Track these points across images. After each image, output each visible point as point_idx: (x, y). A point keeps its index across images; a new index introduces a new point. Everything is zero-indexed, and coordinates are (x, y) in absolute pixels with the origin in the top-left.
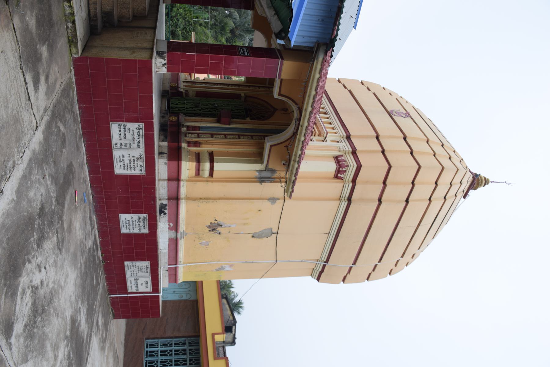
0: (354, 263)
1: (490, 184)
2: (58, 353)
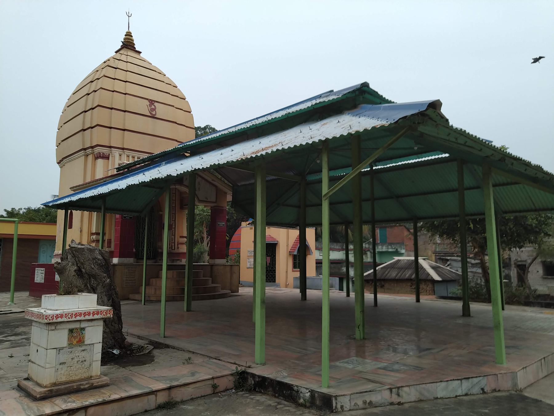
0: (173, 106)
1: (130, 30)
2: (253, 375)
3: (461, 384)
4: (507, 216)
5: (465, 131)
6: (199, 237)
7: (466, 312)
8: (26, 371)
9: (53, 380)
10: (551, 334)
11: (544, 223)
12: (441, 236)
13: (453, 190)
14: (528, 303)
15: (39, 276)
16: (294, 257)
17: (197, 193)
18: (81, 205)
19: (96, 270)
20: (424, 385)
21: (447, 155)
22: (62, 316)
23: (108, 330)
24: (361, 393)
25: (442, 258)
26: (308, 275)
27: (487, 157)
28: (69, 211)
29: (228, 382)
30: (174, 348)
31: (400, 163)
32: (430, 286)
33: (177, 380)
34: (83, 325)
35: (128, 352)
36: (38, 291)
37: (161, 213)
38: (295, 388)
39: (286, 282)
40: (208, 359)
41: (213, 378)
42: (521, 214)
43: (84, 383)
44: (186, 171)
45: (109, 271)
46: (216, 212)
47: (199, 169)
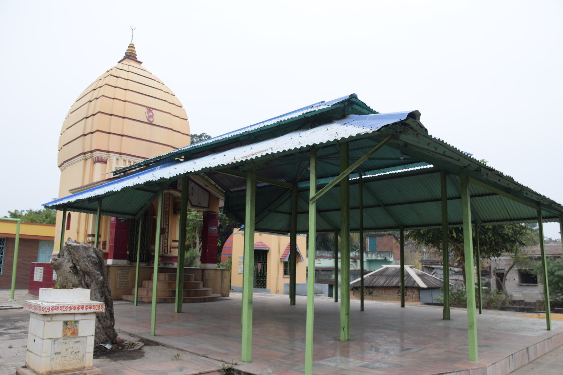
0: (170, 114)
1: (133, 43)
4: (489, 226)
5: (443, 141)
6: (192, 242)
7: (446, 316)
8: (23, 361)
9: (49, 369)
10: (520, 334)
12: (426, 244)
13: (437, 200)
16: (286, 264)
17: (190, 198)
19: (90, 268)
21: (432, 166)
22: (57, 308)
23: (100, 326)
25: (428, 267)
26: (297, 281)
27: (465, 167)
30: (163, 345)
32: (416, 292)
34: (77, 318)
35: (120, 348)
36: (34, 288)
37: (155, 217)
39: (277, 288)
42: (498, 223)
45: (102, 269)
46: (209, 218)
47: (191, 172)
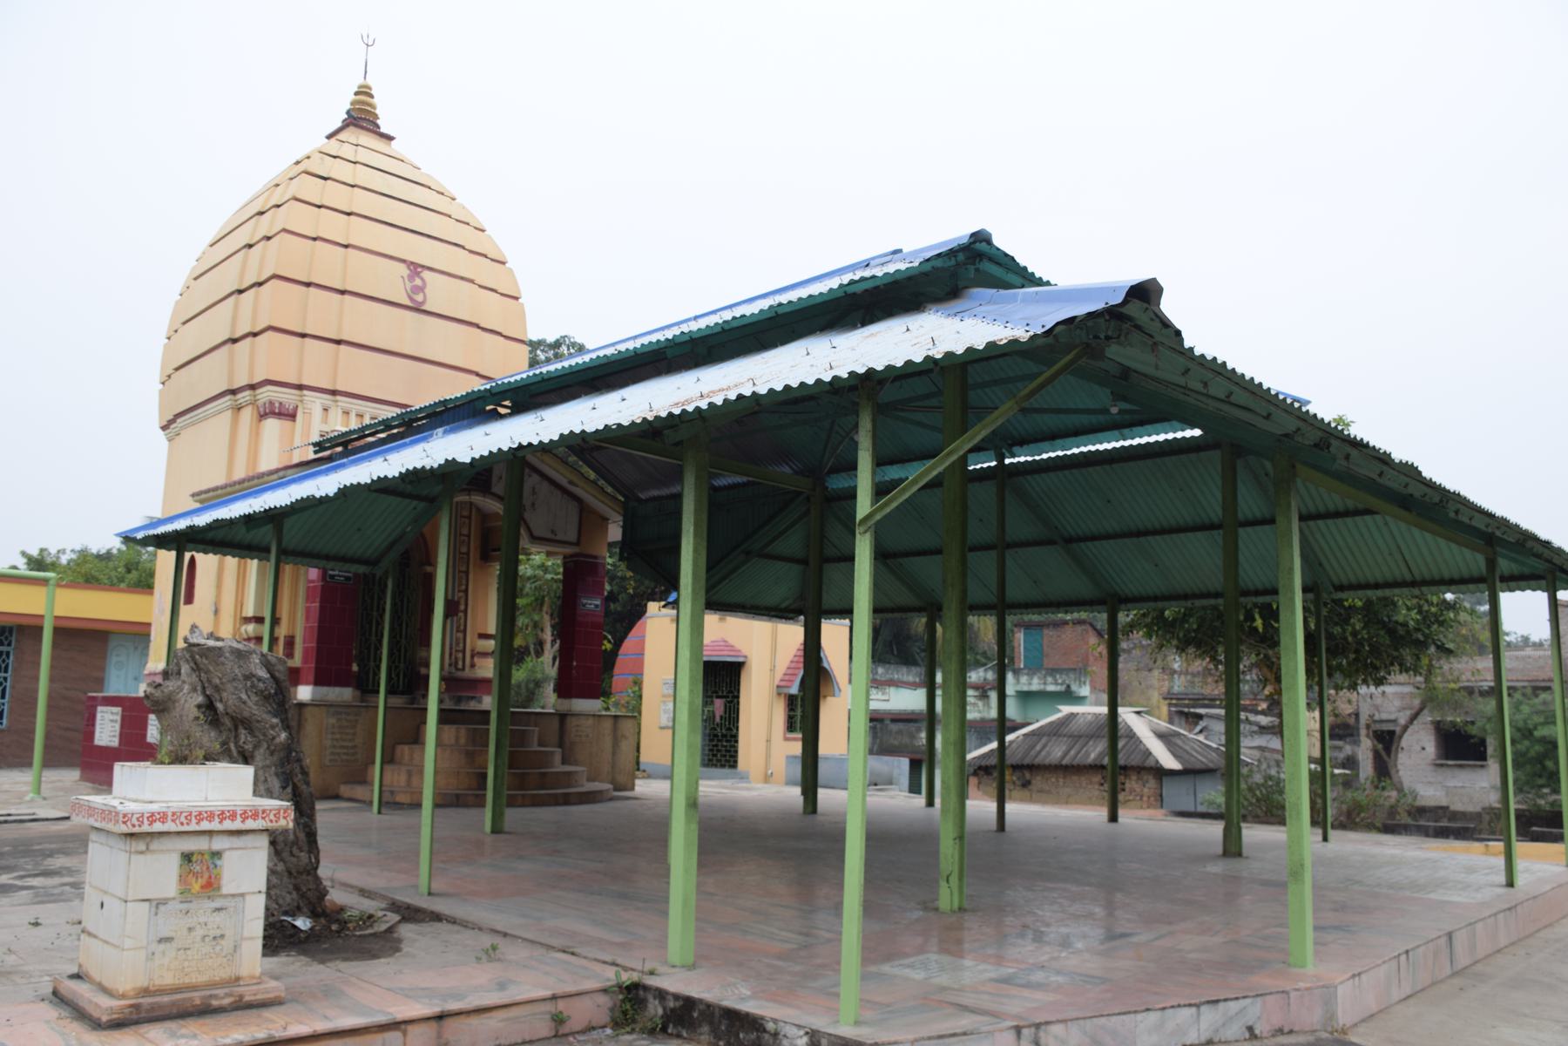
0: (472, 281)
1: (369, 81)
2: (661, 994)
3: (1199, 1014)
6: (531, 640)
7: (1232, 847)
9: (142, 982)
11: (1437, 621)
13: (1212, 527)
14: (1390, 828)
15: (107, 728)
16: (791, 701)
17: (527, 515)
18: (217, 538)
19: (253, 707)
20: (1103, 1020)
21: (1197, 432)
22: (163, 817)
23: (280, 867)
24: (941, 1037)
25: (1186, 712)
26: (823, 749)
27: (1286, 435)
28: (187, 556)
29: (596, 1009)
30: (453, 921)
31: (1076, 451)
32: (1152, 783)
33: (457, 996)
34: (218, 844)
35: (334, 927)
37: (429, 569)
38: (770, 1026)
39: (767, 768)
40: (542, 951)
41: (554, 998)
42: (1379, 593)
43: (220, 992)
44: (495, 450)
46: (580, 572)
47: (530, 444)
